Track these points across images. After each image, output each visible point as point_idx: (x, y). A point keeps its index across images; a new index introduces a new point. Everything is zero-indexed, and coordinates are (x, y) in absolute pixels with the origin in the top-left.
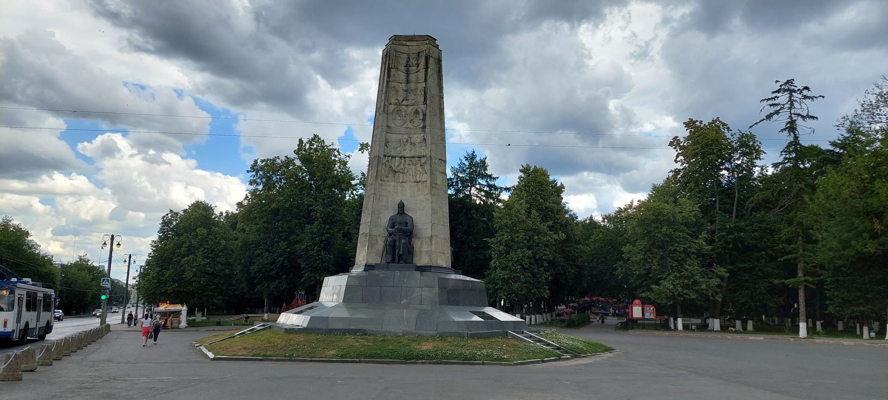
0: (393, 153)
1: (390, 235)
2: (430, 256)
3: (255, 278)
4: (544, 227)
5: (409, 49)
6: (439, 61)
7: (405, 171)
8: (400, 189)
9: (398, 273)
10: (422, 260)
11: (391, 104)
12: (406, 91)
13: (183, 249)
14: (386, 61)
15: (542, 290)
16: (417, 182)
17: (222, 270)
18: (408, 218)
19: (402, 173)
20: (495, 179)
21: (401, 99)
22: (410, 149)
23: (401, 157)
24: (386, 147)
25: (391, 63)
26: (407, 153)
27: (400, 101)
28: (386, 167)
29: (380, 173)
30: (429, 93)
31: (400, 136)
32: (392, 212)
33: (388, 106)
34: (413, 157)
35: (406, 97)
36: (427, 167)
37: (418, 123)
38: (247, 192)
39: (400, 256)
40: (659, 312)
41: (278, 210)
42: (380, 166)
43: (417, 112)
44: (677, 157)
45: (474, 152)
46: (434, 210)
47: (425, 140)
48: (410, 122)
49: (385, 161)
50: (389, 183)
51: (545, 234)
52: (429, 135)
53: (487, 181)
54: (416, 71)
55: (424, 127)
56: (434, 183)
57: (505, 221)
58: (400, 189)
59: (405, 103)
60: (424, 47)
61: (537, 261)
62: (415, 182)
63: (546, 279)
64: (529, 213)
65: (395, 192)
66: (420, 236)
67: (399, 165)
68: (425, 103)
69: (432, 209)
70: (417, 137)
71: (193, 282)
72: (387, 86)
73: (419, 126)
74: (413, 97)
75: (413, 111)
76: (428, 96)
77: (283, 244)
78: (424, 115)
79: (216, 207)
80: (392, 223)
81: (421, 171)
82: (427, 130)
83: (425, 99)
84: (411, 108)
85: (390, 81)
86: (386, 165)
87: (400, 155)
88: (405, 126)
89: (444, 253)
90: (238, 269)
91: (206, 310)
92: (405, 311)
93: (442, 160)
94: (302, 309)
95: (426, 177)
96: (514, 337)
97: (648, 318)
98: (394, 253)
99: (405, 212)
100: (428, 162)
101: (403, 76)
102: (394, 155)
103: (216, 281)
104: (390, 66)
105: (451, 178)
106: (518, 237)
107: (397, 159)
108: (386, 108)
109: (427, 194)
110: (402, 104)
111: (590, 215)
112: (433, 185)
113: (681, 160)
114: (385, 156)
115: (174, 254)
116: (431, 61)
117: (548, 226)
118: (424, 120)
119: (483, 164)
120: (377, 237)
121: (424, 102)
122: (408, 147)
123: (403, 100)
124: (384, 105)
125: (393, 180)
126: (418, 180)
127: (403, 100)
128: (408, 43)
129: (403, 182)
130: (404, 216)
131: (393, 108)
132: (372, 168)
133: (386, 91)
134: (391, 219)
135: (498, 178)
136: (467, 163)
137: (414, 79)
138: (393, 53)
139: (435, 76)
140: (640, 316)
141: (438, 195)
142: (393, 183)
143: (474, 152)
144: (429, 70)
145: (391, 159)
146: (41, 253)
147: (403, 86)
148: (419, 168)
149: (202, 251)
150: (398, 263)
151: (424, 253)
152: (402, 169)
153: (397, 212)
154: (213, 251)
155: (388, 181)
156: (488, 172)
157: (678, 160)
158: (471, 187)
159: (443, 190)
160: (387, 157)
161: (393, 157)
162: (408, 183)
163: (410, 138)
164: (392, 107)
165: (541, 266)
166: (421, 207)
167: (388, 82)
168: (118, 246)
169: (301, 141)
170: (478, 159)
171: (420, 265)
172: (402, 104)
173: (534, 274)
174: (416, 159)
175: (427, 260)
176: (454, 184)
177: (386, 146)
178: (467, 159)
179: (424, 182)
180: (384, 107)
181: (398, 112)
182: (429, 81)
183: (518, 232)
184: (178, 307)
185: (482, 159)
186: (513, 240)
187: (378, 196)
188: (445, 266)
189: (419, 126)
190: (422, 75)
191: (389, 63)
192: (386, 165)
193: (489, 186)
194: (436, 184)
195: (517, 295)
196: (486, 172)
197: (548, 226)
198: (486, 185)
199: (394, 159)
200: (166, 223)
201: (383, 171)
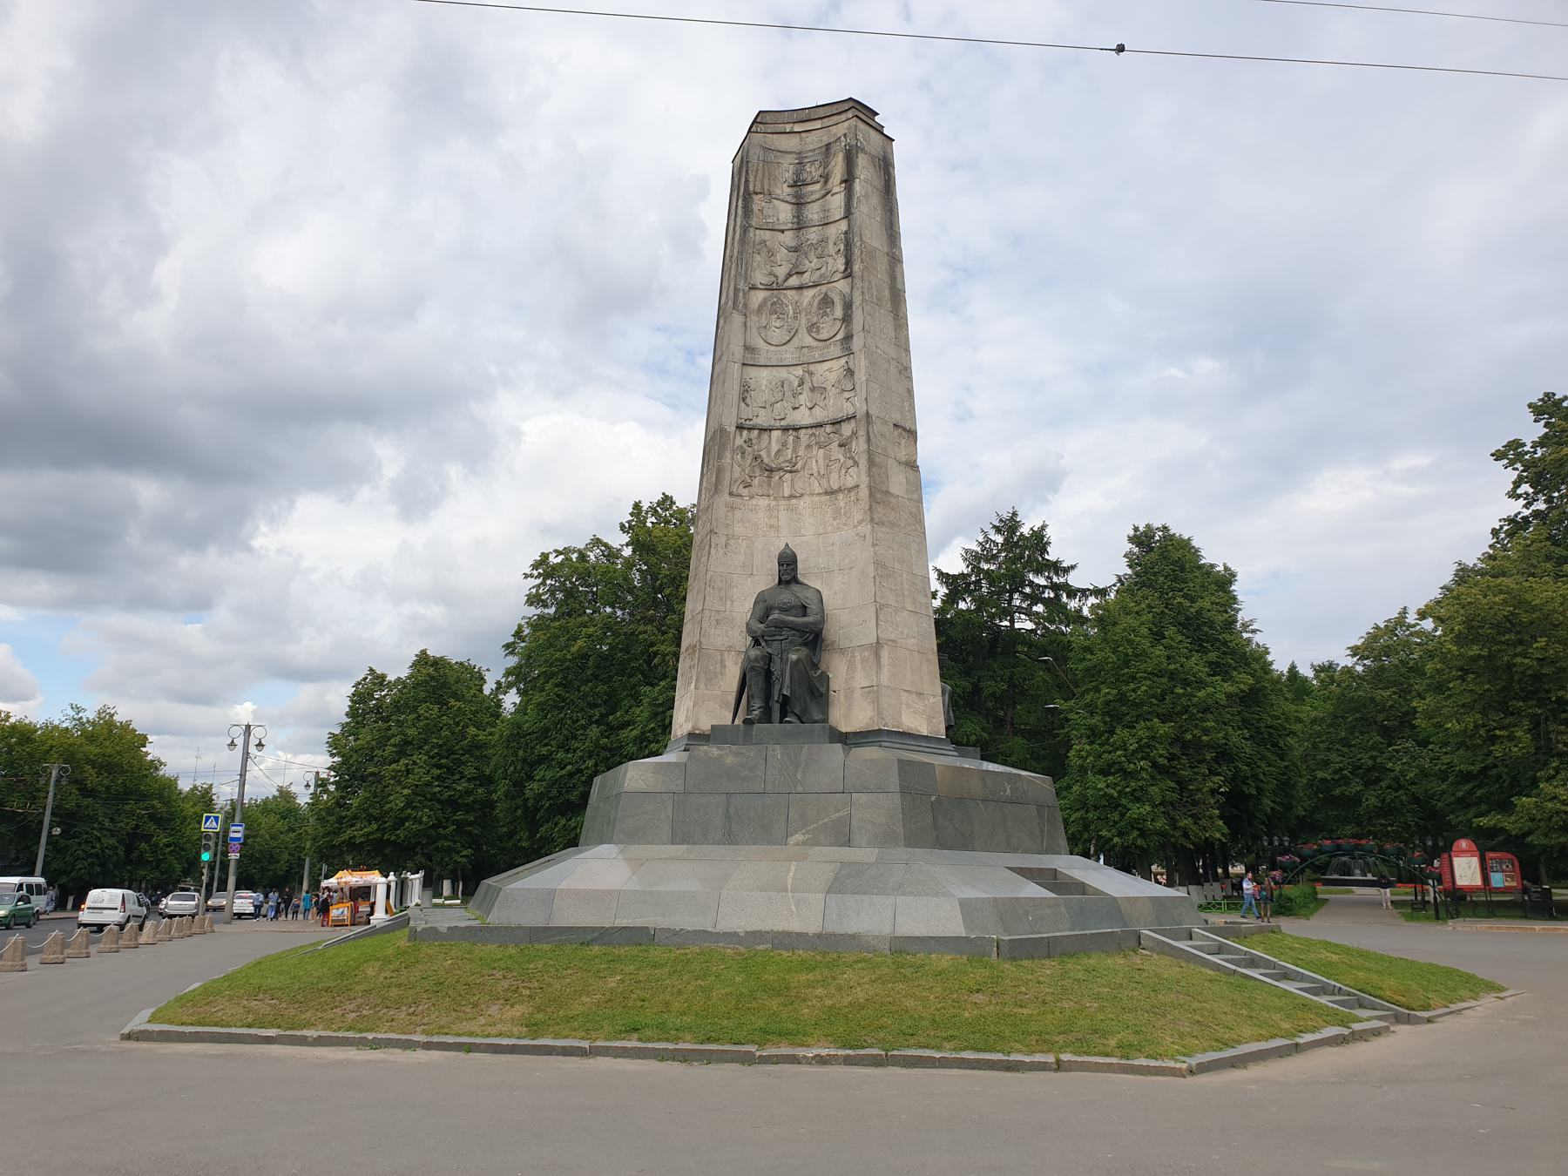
0: (763, 419)
1: (756, 642)
2: (876, 702)
3: (536, 810)
4: (1196, 664)
5: (801, 139)
6: (885, 166)
7: (799, 466)
8: (783, 515)
9: (777, 752)
10: (850, 713)
11: (753, 288)
12: (795, 250)
13: (389, 749)
14: (739, 181)
15: (1204, 822)
16: (832, 493)
17: (468, 792)
18: (809, 594)
19: (791, 472)
20: (1067, 570)
21: (781, 272)
22: (810, 405)
23: (785, 429)
24: (743, 404)
25: (751, 179)
26: (803, 417)
27: (781, 278)
28: (743, 457)
29: (728, 474)
30: (858, 244)
31: (783, 373)
32: (765, 578)
34: (820, 425)
35: (795, 266)
36: (859, 446)
37: (830, 327)
38: (523, 622)
39: (785, 702)
40: (1528, 872)
41: (585, 656)
43: (826, 301)
44: (1517, 484)
45: (1015, 514)
46: (884, 567)
47: (850, 372)
48: (809, 331)
50: (754, 501)
51: (1201, 684)
52: (863, 357)
53: (1049, 578)
54: (823, 192)
55: (849, 337)
56: (880, 491)
57: (1100, 655)
58: (783, 515)
59: (794, 281)
60: (840, 130)
61: (1185, 747)
62: (826, 493)
63: (1213, 792)
64: (1158, 636)
65: (771, 526)
66: (844, 644)
67: (779, 451)
68: (848, 274)
69: (878, 564)
70: (829, 372)
71: (407, 819)
72: (743, 241)
73: (838, 337)
74: (815, 263)
75: (819, 298)
76: (857, 252)
77: (594, 731)
78: (848, 306)
79: (488, 670)
80: (764, 609)
81: (842, 459)
82: (857, 343)
83: (848, 263)
84: (809, 293)
85: (750, 226)
86: (743, 453)
87: (783, 423)
88: (795, 343)
89: (919, 694)
90: (502, 788)
91: (461, 883)
92: (793, 868)
93: (904, 429)
95: (857, 476)
96: (1163, 949)
97: (1501, 885)
98: (767, 697)
99: (800, 578)
100: (862, 433)
101: (785, 213)
102: (765, 425)
103: (459, 816)
104: (751, 188)
105: (963, 574)
106: (1134, 690)
107: (775, 434)
109: (860, 522)
110: (786, 284)
112: (879, 496)
113: (1525, 493)
114: (740, 428)
116: (862, 161)
117: (1210, 664)
118: (847, 318)
119: (1039, 541)
120: (722, 655)
121: (846, 269)
122: (803, 399)
123: (789, 275)
124: (736, 290)
125: (766, 492)
126: (835, 487)
127: (789, 275)
128: (797, 128)
129: (791, 497)
130: (794, 587)
131: (760, 299)
132: (707, 467)
133: (741, 253)
134: (760, 599)
135: (1073, 567)
136: (1000, 539)
137: (816, 217)
138: (756, 154)
139: (875, 200)
140: (1478, 882)
141: (893, 525)
142: (764, 502)
143: (1015, 514)
144: (858, 186)
145: (759, 436)
146: (166, 775)
147: (788, 238)
148: (837, 453)
149: (427, 754)
150: (781, 722)
151: (858, 693)
152: (790, 461)
153: (777, 582)
154: (451, 752)
155: (752, 497)
156: (1052, 556)
157: (1519, 491)
158: (1011, 592)
159: (911, 513)
160: (745, 432)
161: (762, 430)
162: (806, 499)
163: (811, 374)
164: (758, 297)
165: (1200, 762)
166: (847, 561)
167: (745, 230)
168: (260, 748)
169: (637, 506)
170: (1025, 530)
171: (849, 730)
172: (786, 284)
173: (1182, 785)
174: (828, 429)
175: (869, 714)
176: (972, 587)
177: (744, 400)
178: (998, 530)
179: (850, 490)
180: (736, 296)
181: (776, 309)
182: (856, 215)
183: (1133, 678)
184: (375, 877)
185: (1035, 529)
186: (1122, 698)
187: (724, 539)
188: (925, 733)
189: (838, 337)
190: (837, 202)
191: (747, 181)
192: (743, 453)
193: (1055, 587)
194: (887, 493)
195: (1143, 834)
196: (1047, 557)
197: (1210, 664)
198: (1045, 587)
199: (765, 436)
200: (360, 697)
201: (737, 469)
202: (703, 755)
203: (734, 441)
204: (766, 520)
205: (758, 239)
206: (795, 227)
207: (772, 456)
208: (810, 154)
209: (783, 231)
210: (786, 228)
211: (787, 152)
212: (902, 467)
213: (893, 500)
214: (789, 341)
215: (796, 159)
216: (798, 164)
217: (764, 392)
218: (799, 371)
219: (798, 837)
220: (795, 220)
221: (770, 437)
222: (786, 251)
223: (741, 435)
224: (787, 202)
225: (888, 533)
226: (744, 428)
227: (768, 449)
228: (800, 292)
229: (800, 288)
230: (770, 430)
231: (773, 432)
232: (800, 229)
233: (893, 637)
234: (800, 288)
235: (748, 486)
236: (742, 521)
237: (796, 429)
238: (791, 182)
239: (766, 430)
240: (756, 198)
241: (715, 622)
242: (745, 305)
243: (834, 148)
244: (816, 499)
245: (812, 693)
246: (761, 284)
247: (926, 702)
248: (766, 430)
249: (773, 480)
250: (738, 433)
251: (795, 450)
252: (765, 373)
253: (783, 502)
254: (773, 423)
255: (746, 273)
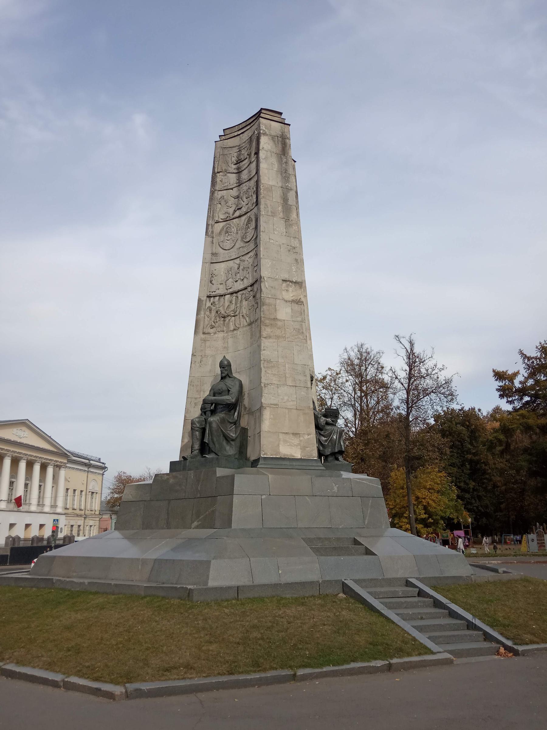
7: (237, 313)
11: (217, 222)
12: (237, 197)
19: (234, 316)
21: (231, 211)
23: (232, 294)
27: (231, 213)
28: (210, 312)
31: (231, 263)
33: (212, 226)
34: (246, 288)
42: (202, 313)
49: (210, 305)
50: (216, 335)
58: (230, 341)
84: (243, 218)
86: (210, 310)
87: (231, 290)
89: (295, 434)
94: (24, 567)
104: (216, 171)
108: (210, 229)
111: (518, 370)
115: (425, 499)
123: (235, 211)
127: (235, 211)
129: (234, 330)
142: (221, 335)
145: (219, 299)
155: (215, 333)
160: (212, 299)
174: (249, 289)
188: (299, 457)
192: (210, 310)
194: (275, 319)
199: (222, 299)
202: (160, 479)
203: (206, 305)
204: (222, 344)
205: (219, 197)
206: (238, 185)
207: (226, 309)
208: (244, 144)
209: (232, 189)
210: (233, 187)
211: (233, 147)
212: (289, 304)
213: (279, 323)
214: (234, 245)
215: (238, 149)
216: (239, 151)
217: (222, 275)
218: (237, 261)
219: (196, 523)
220: (238, 181)
221: (224, 299)
222: (234, 199)
223: (210, 301)
224: (233, 173)
225: (274, 342)
226: (211, 297)
227: (223, 306)
228: (240, 218)
229: (240, 216)
230: (225, 295)
231: (226, 296)
232: (240, 185)
233: (275, 402)
234: (240, 216)
235: (212, 327)
236: (210, 347)
237: (236, 293)
238: (235, 162)
239: (222, 296)
240: (218, 174)
241: (193, 405)
242: (212, 232)
243: (253, 138)
244: (245, 329)
245: (226, 439)
246: (221, 219)
247: (301, 438)
248: (222, 296)
249: (225, 322)
250: (208, 299)
251: (236, 304)
252: (223, 265)
253: (230, 334)
254: (226, 291)
255: (213, 215)
